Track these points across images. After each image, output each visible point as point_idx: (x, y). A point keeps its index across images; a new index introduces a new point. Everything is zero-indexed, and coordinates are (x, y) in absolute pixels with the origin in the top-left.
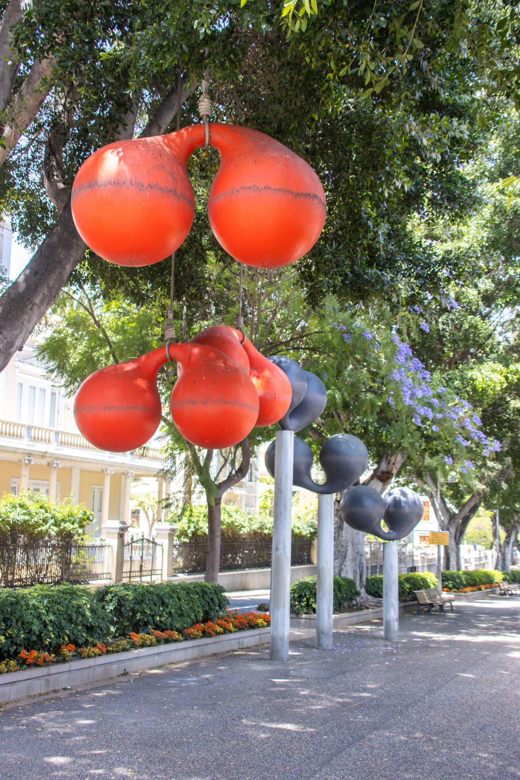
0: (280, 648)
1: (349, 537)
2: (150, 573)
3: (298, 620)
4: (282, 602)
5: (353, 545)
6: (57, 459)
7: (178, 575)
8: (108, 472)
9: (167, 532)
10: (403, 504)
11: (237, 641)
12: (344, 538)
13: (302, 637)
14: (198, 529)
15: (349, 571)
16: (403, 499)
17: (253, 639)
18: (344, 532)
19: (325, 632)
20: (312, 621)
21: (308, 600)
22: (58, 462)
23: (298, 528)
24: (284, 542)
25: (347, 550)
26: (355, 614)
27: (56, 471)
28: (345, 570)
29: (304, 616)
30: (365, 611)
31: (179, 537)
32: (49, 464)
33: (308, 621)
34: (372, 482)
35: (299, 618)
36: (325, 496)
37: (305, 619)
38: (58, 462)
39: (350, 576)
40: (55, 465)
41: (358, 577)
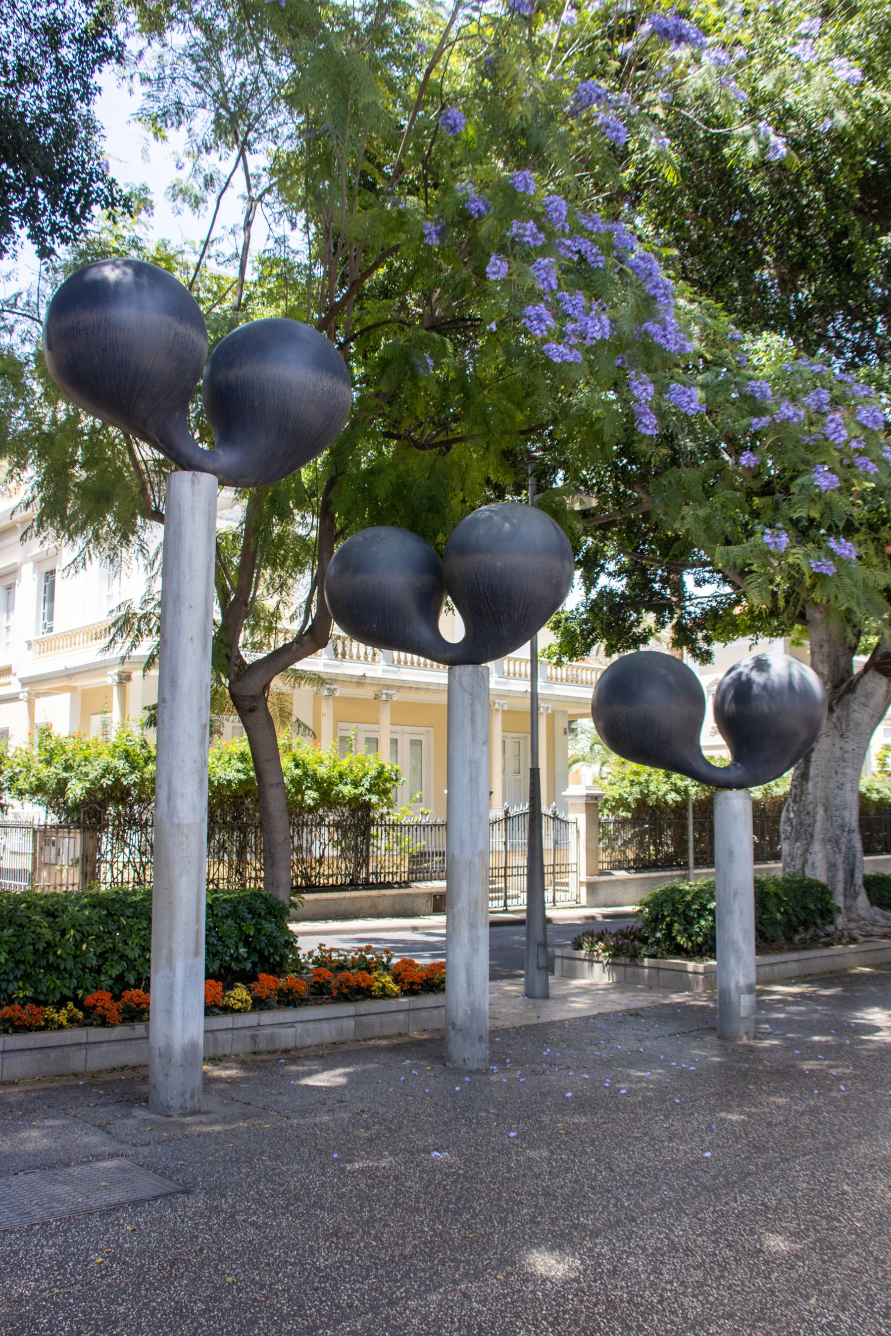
0: (161, 1078)
1: (819, 794)
2: (509, 872)
3: (636, 969)
4: (165, 952)
5: (826, 810)
6: (389, 687)
7: (614, 872)
8: (497, 706)
9: (583, 801)
10: (756, 690)
11: (249, 1033)
12: (810, 797)
13: (730, 996)
14: (647, 795)
15: (817, 864)
16: (758, 678)
17: (325, 1027)
18: (810, 785)
19: (458, 1023)
20: (661, 973)
21: (670, 926)
22: (390, 692)
23: (878, 792)
24: (170, 784)
25: (815, 821)
26: (795, 956)
27: (388, 706)
28: (810, 862)
29: (646, 961)
30: (838, 948)
31: (613, 810)
32: (377, 697)
33: (653, 972)
34: (866, 677)
35: (637, 965)
36: (457, 668)
37: (648, 967)
38: (390, 692)
39: (819, 874)
40: (384, 697)
41: (841, 876)
